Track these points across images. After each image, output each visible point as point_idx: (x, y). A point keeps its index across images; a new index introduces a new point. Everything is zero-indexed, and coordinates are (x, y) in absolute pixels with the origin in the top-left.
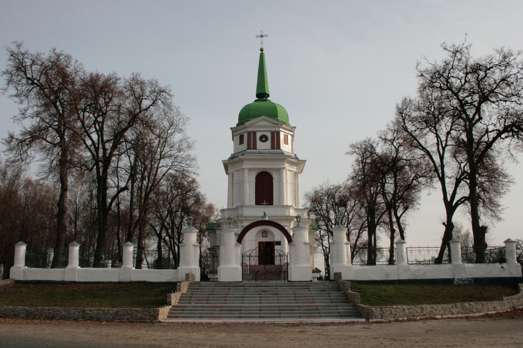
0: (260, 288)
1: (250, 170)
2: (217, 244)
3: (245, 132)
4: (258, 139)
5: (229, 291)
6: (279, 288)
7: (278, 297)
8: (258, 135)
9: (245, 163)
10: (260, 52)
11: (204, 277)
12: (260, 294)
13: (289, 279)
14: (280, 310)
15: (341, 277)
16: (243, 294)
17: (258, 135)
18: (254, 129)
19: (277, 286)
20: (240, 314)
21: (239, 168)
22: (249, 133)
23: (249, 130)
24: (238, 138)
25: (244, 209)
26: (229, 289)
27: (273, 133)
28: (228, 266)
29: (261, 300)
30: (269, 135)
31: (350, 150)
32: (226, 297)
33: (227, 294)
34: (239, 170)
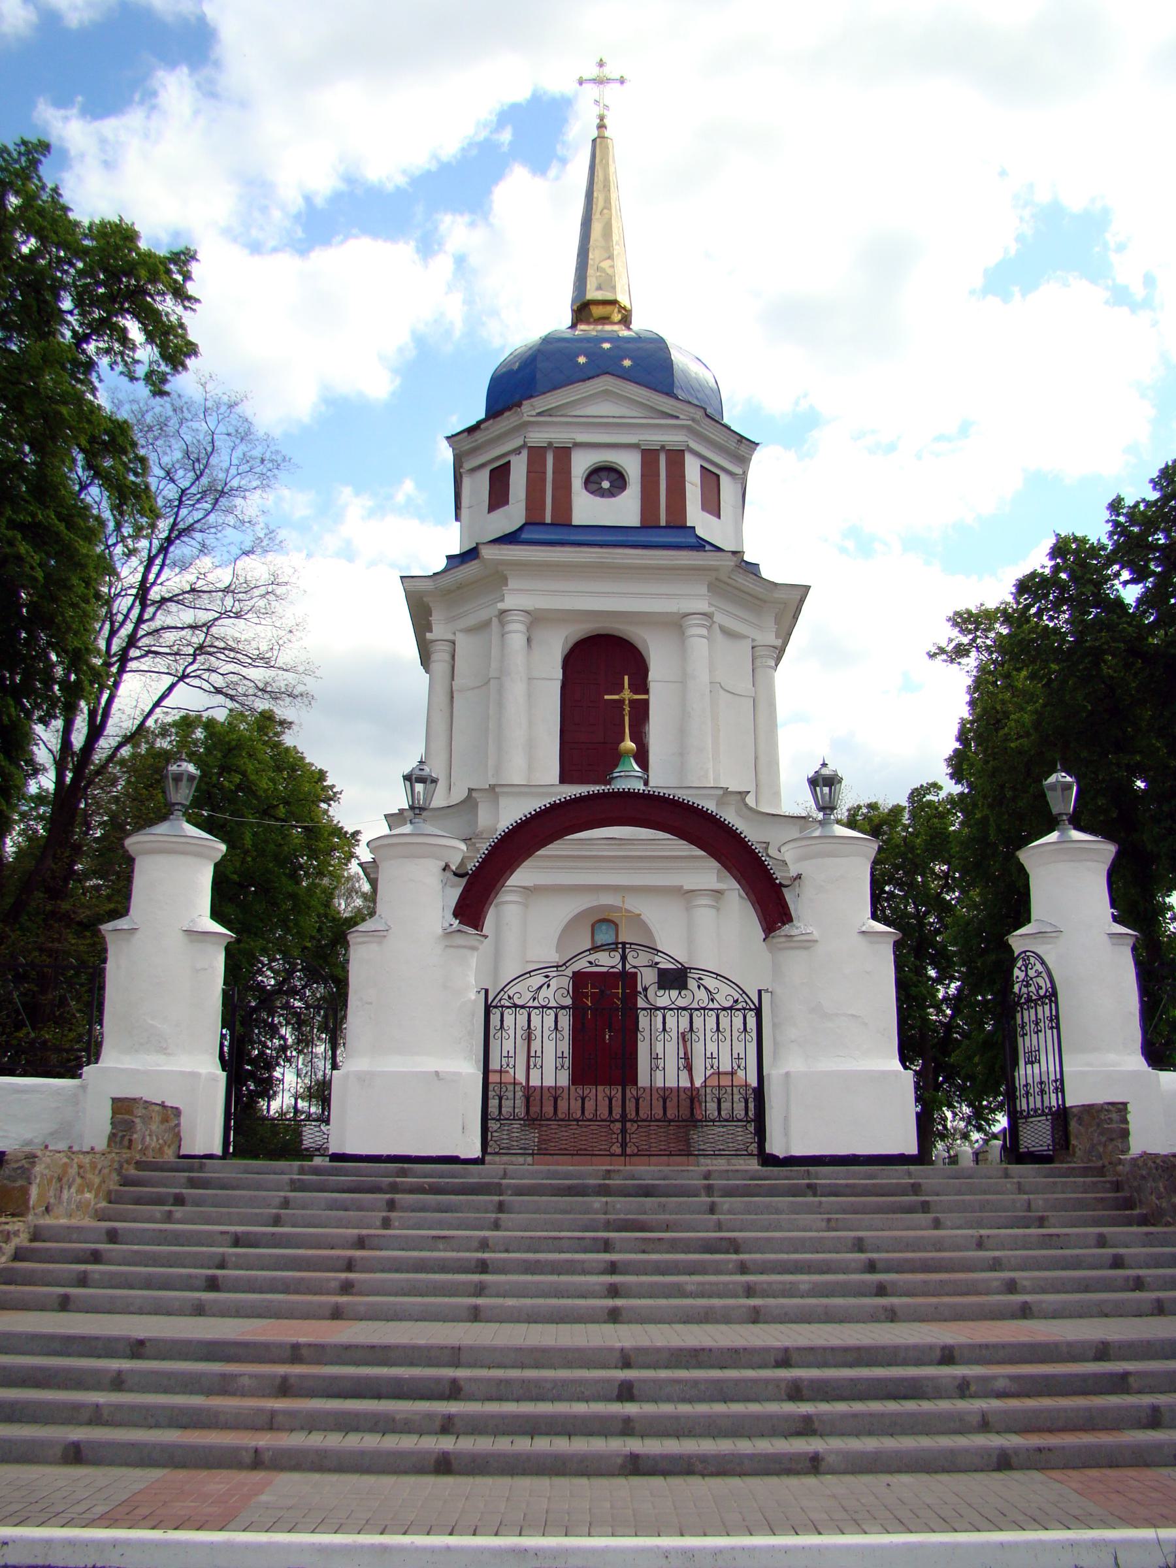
0: (598, 1202)
1: (536, 620)
2: (617, 1354)
3: (517, 451)
4: (577, 483)
5: (386, 1223)
6: (725, 1202)
7: (743, 1269)
8: (581, 463)
9: (513, 584)
10: (595, 134)
11: (253, 1132)
12: (607, 1246)
13: (776, 1146)
14: (796, 1392)
15: (1125, 1134)
16: (484, 1245)
17: (581, 463)
18: (560, 436)
19: (709, 1190)
20: (447, 1426)
21: (484, 615)
22: (536, 455)
23: (538, 437)
24: (479, 486)
25: (503, 802)
26: (391, 1205)
27: (649, 457)
28: (395, 1064)
29: (614, 1291)
30: (631, 465)
31: (949, 635)
32: (350, 1266)
33: (361, 1243)
34: (485, 625)
